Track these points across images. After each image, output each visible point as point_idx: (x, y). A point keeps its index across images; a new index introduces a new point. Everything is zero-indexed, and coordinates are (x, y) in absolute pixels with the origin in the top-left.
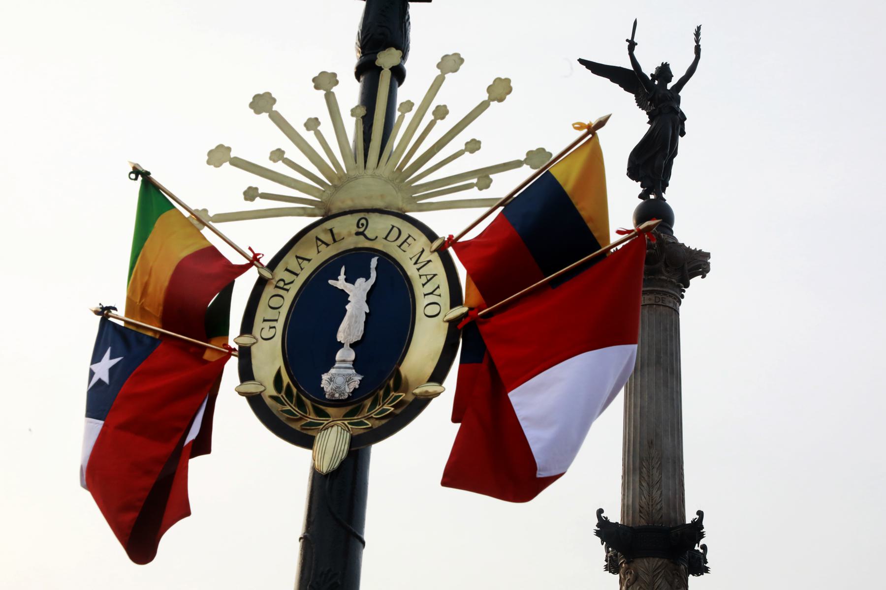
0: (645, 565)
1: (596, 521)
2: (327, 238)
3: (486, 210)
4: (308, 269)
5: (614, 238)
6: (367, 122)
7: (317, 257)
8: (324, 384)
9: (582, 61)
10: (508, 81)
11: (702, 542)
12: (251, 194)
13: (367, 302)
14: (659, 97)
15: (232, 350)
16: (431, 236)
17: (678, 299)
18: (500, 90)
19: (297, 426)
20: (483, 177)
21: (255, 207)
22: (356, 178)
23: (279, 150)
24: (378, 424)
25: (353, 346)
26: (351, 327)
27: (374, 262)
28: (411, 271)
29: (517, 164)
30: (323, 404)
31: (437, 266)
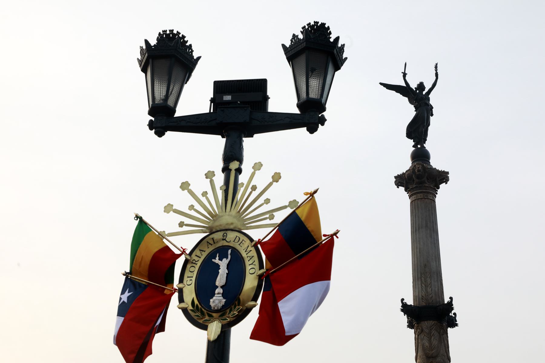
0: (426, 324)
1: (401, 304)
2: (211, 242)
3: (273, 228)
4: (205, 255)
5: (323, 238)
6: (226, 192)
8: (212, 304)
9: (381, 84)
10: (279, 173)
11: (453, 312)
12: (181, 224)
13: (227, 268)
15: (175, 289)
16: (251, 240)
18: (277, 177)
20: (271, 214)
24: (232, 319)
26: (221, 280)
27: (230, 251)
28: (244, 255)
29: (285, 207)
31: (254, 253)
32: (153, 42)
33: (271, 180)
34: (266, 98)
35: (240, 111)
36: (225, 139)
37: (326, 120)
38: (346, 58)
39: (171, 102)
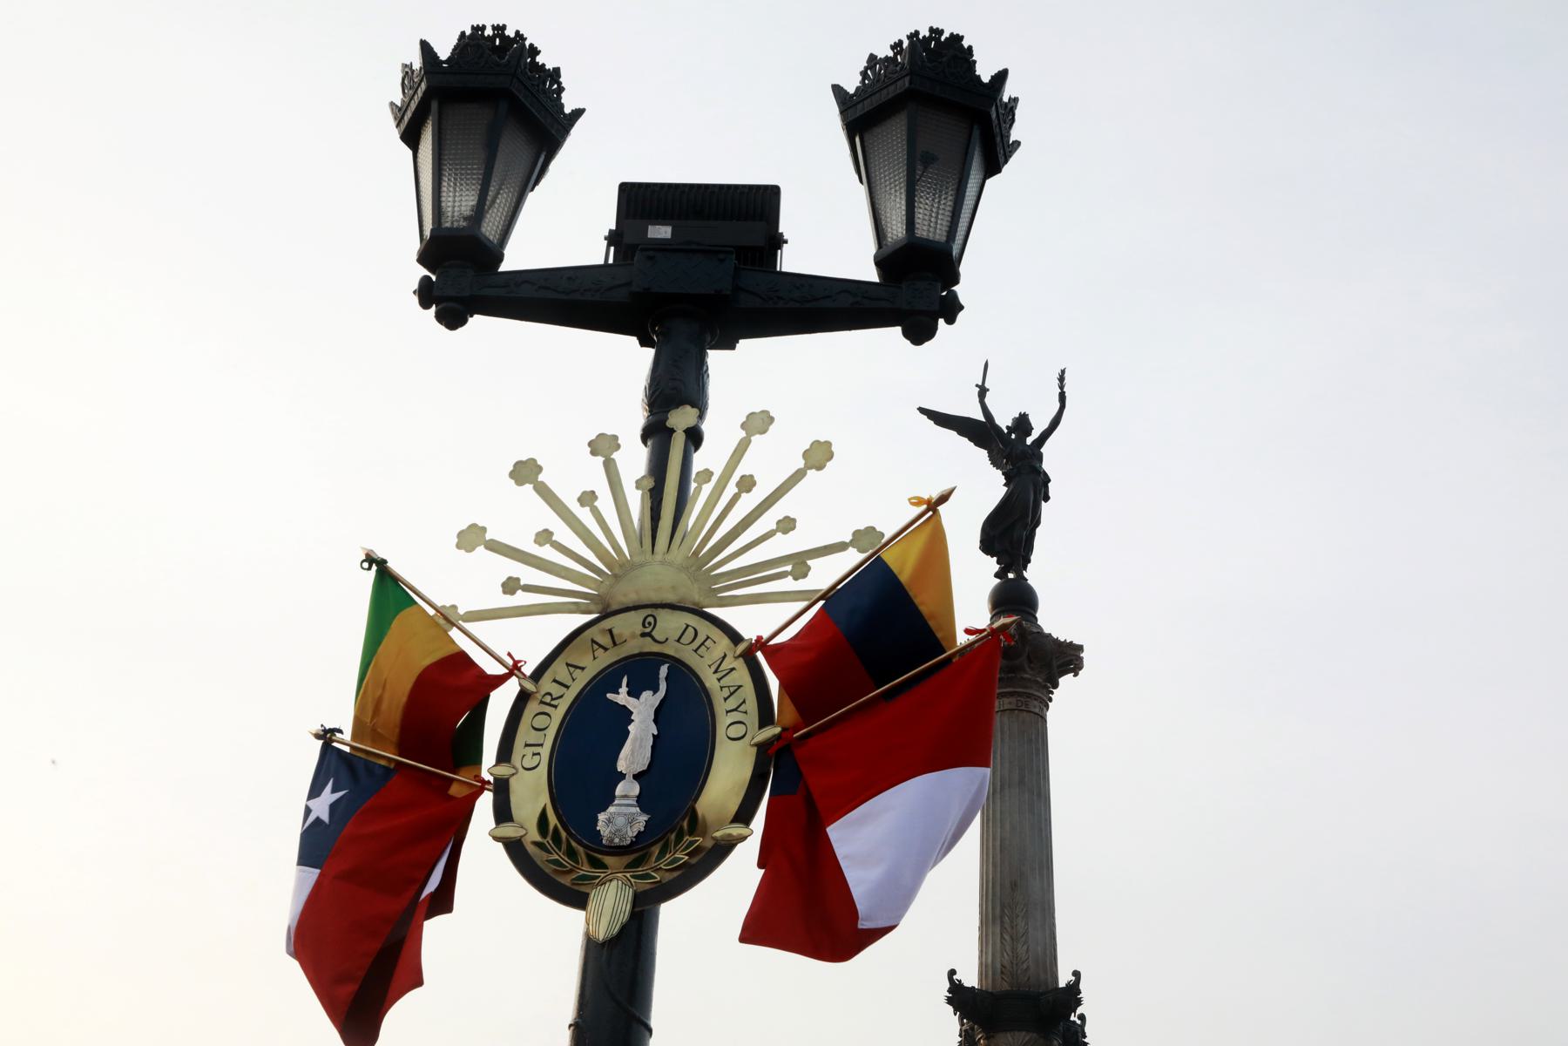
4: (582, 679)
5: (962, 639)
6: (655, 496)
7: (593, 664)
8: (601, 826)
9: (922, 411)
10: (828, 444)
11: (1079, 1011)
13: (655, 721)
14: (1016, 453)
16: (735, 637)
17: (1045, 703)
18: (818, 456)
19: (566, 881)
20: (799, 563)
21: (517, 603)
22: (642, 565)
23: (546, 531)
24: (669, 877)
25: (636, 777)
26: (634, 754)
27: (664, 671)
28: (711, 682)
30: (598, 852)
31: (742, 676)
32: (444, 51)
33: (801, 464)
34: (777, 241)
35: (696, 274)
36: (650, 353)
37: (962, 308)
38: (1017, 144)
39: (490, 228)
